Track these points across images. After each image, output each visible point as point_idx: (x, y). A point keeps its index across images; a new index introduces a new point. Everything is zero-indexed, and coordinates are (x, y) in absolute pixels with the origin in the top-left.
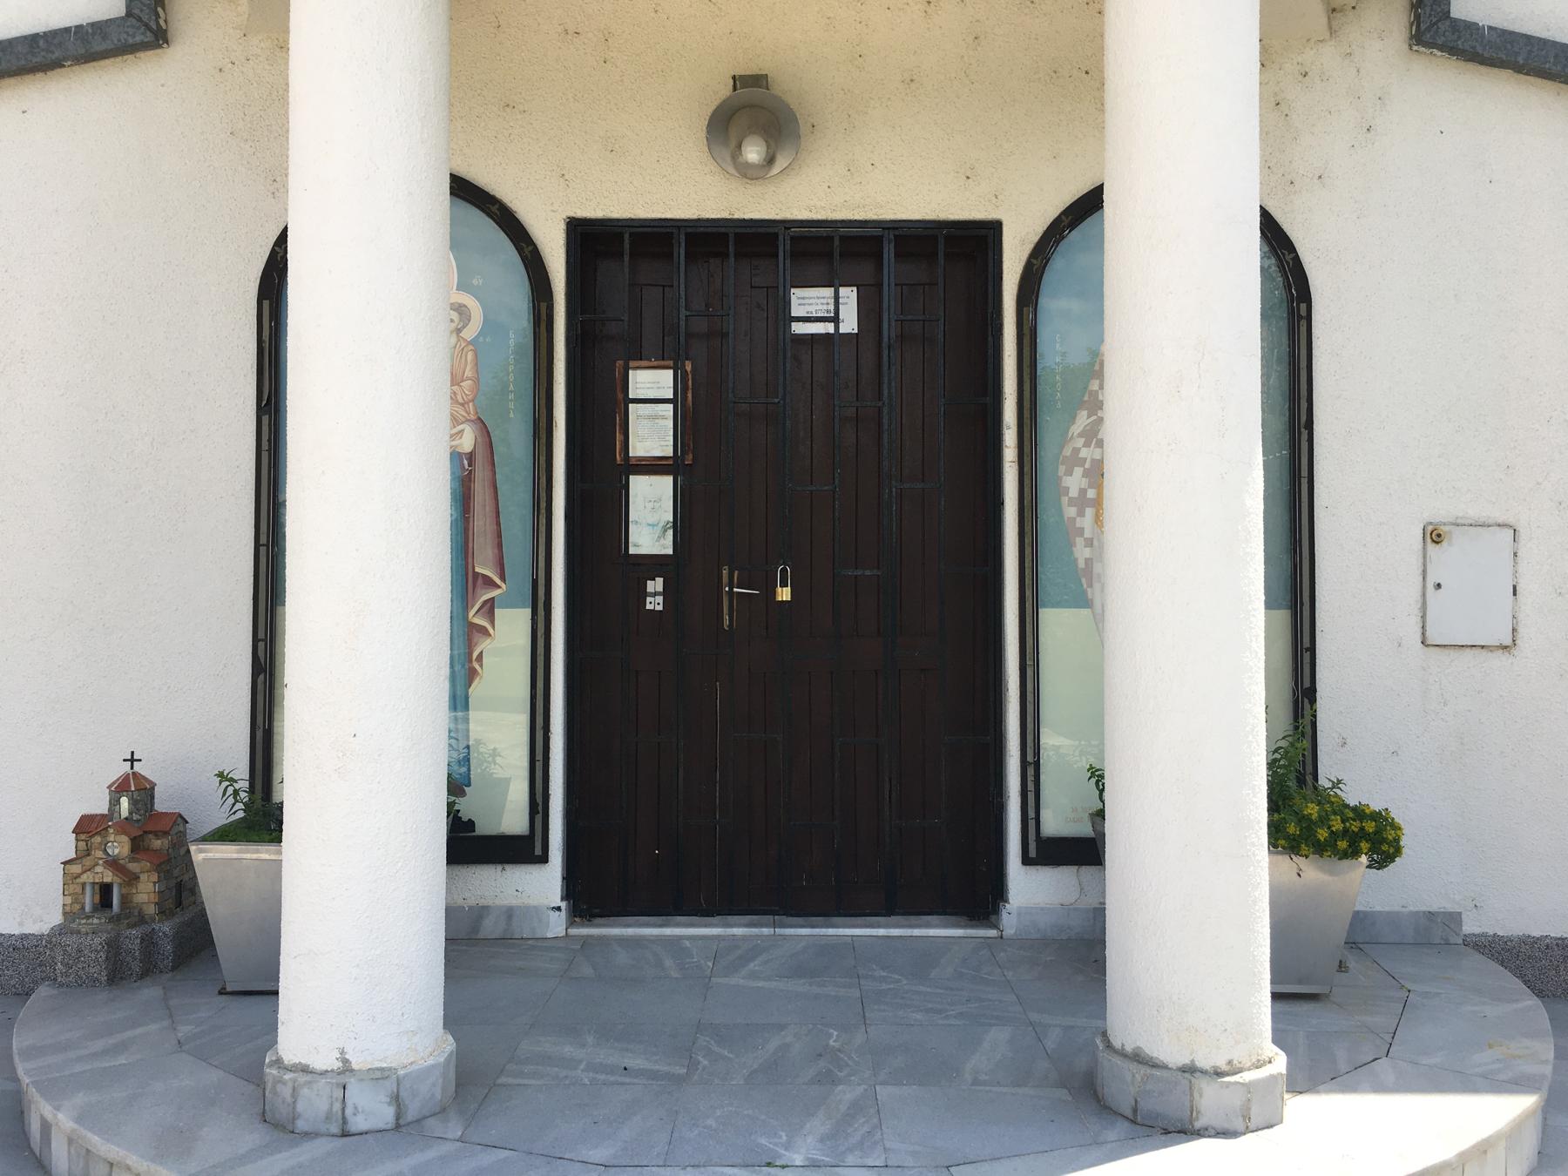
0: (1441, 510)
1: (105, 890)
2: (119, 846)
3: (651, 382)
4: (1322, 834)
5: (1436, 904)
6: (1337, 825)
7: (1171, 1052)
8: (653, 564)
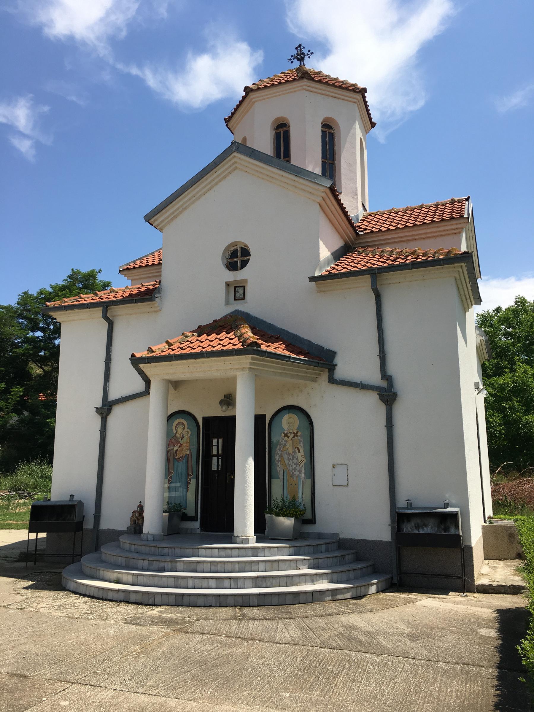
0: (336, 462)
2: (137, 515)
5: (335, 532)
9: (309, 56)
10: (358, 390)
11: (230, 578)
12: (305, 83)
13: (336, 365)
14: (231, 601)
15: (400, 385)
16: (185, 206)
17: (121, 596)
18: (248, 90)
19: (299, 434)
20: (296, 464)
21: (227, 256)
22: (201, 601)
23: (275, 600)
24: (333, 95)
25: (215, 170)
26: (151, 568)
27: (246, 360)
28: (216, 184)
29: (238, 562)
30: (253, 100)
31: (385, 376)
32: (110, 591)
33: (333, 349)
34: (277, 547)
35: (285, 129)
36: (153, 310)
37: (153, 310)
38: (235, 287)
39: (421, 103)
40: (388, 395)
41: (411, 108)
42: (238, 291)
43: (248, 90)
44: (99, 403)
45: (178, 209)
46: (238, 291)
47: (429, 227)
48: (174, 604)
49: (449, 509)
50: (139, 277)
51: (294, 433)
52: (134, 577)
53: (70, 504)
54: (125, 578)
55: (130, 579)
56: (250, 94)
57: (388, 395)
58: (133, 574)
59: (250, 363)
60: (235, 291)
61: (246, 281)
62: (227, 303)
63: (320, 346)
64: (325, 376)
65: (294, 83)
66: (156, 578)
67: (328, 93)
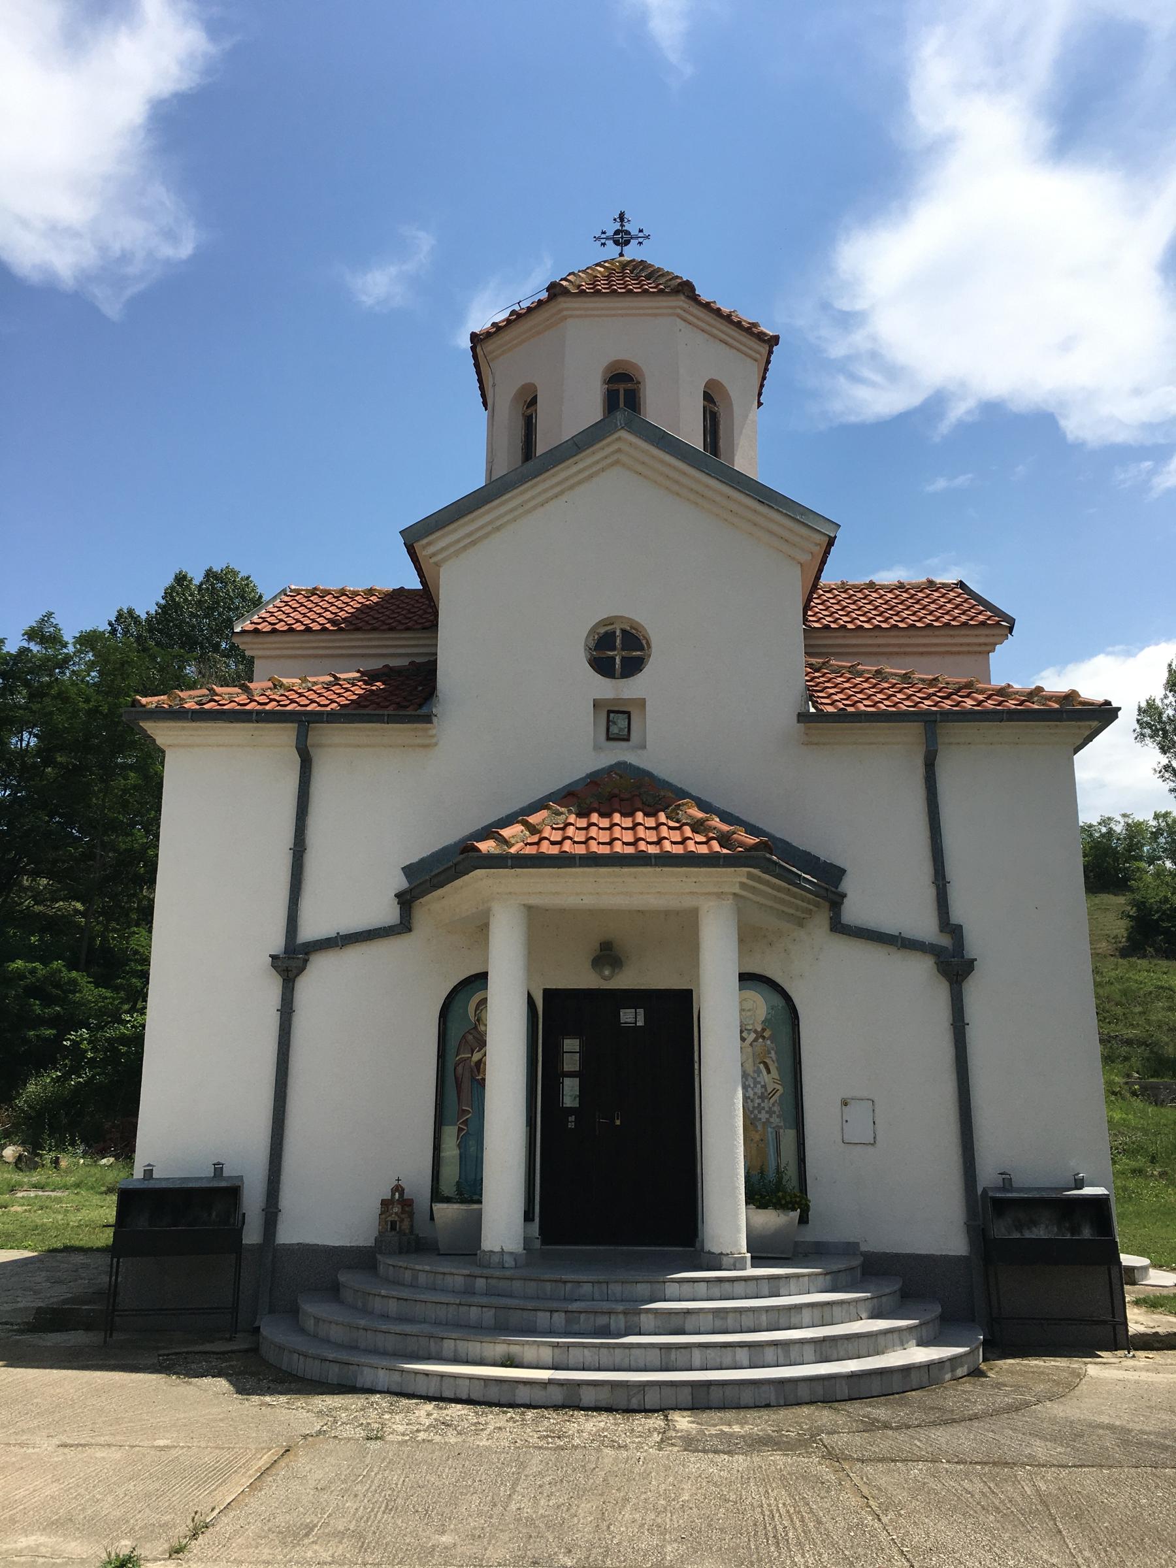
1: (393, 1223)
3: (571, 1044)
4: (783, 1202)
5: (852, 1240)
6: (788, 1199)
7: (716, 1250)
8: (571, 1111)
9: (641, 240)
10: (892, 949)
11: (775, 1344)
12: (681, 303)
13: (844, 896)
14: (803, 1392)
15: (975, 945)
16: (498, 523)
17: (557, 1395)
18: (557, 290)
19: (766, 1034)
20: (762, 1097)
21: (592, 644)
22: (747, 1396)
23: (876, 1385)
24: (724, 337)
25: (575, 458)
26: (576, 1328)
27: (734, 878)
28: (571, 488)
29: (767, 1309)
30: (565, 313)
31: (947, 925)
32: (521, 1386)
33: (839, 863)
34: (809, 1275)
35: (629, 386)
36: (419, 741)
37: (419, 741)
38: (609, 712)
39: (185, 250)
40: (954, 964)
41: (167, 251)
42: (617, 721)
43: (557, 290)
44: (277, 943)
45: (482, 527)
46: (617, 721)
47: (937, 633)
48: (690, 1405)
49: (1088, 1191)
50: (278, 652)
51: (756, 1031)
52: (557, 1351)
53: (215, 1184)
54: (529, 1354)
55: (546, 1354)
56: (561, 299)
57: (954, 964)
58: (557, 1345)
59: (743, 885)
60: (608, 721)
61: (641, 703)
62: (597, 748)
63: (809, 854)
64: (821, 920)
65: (660, 298)
66: (617, 1351)
67: (715, 332)
